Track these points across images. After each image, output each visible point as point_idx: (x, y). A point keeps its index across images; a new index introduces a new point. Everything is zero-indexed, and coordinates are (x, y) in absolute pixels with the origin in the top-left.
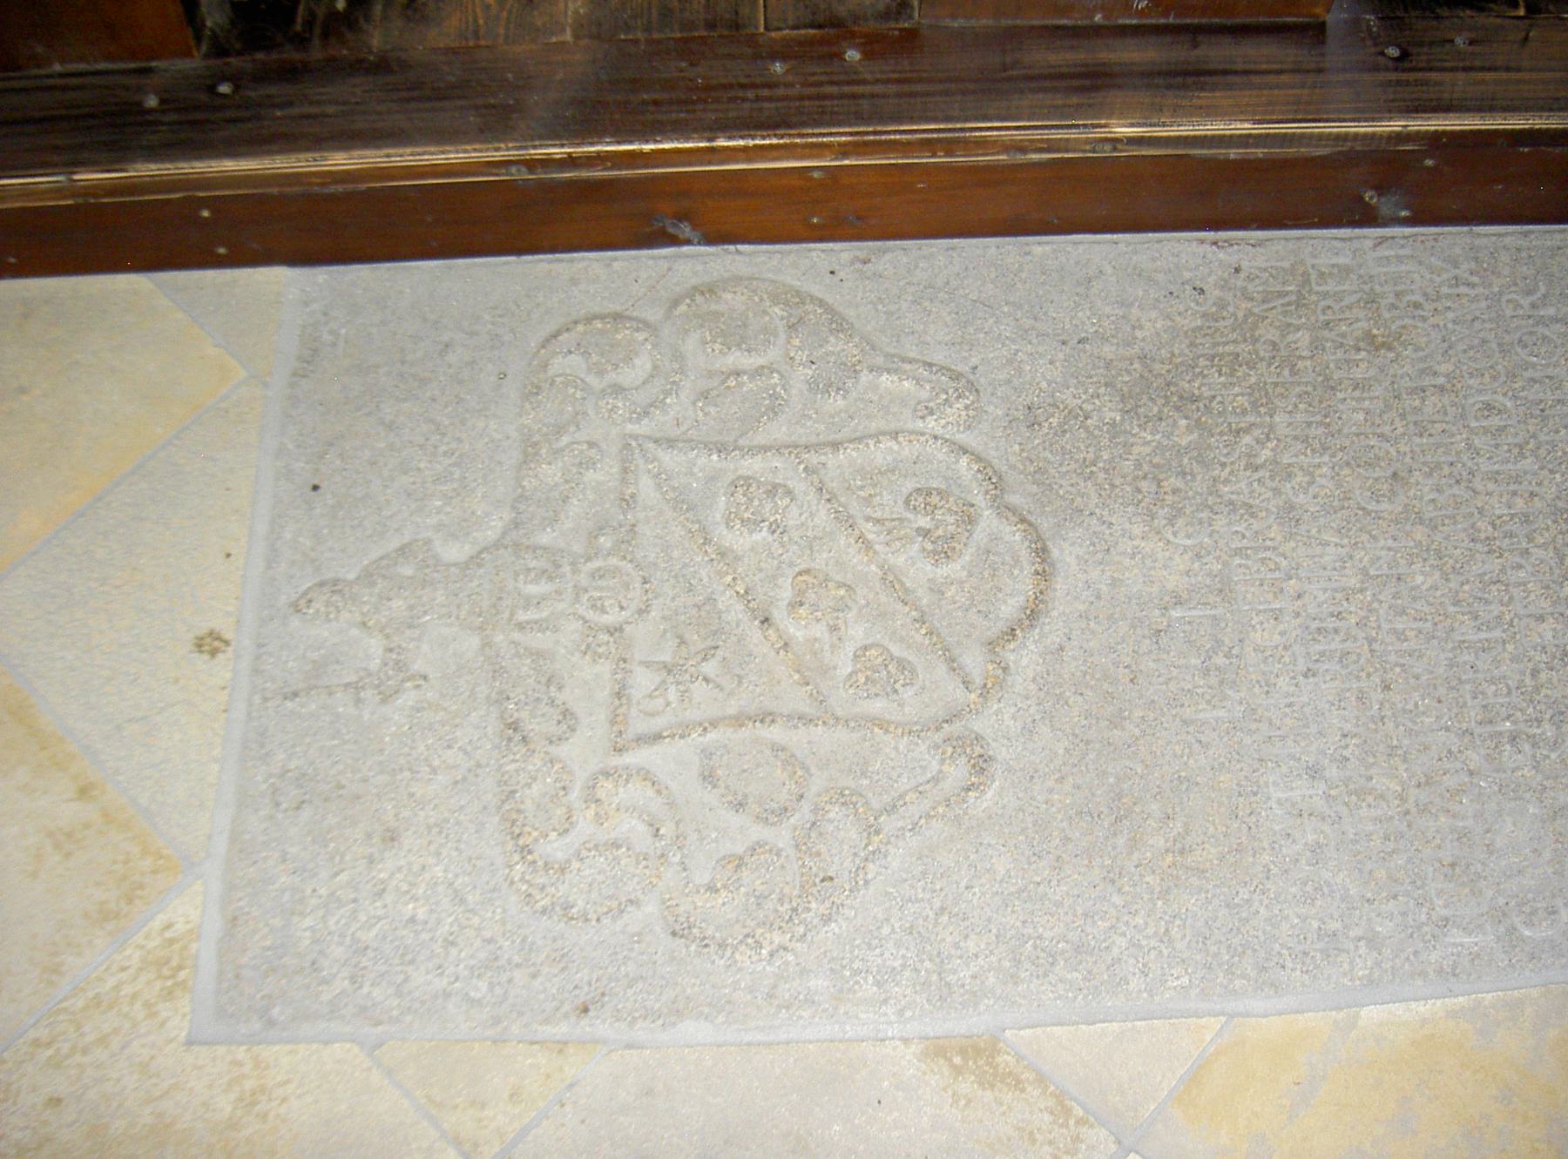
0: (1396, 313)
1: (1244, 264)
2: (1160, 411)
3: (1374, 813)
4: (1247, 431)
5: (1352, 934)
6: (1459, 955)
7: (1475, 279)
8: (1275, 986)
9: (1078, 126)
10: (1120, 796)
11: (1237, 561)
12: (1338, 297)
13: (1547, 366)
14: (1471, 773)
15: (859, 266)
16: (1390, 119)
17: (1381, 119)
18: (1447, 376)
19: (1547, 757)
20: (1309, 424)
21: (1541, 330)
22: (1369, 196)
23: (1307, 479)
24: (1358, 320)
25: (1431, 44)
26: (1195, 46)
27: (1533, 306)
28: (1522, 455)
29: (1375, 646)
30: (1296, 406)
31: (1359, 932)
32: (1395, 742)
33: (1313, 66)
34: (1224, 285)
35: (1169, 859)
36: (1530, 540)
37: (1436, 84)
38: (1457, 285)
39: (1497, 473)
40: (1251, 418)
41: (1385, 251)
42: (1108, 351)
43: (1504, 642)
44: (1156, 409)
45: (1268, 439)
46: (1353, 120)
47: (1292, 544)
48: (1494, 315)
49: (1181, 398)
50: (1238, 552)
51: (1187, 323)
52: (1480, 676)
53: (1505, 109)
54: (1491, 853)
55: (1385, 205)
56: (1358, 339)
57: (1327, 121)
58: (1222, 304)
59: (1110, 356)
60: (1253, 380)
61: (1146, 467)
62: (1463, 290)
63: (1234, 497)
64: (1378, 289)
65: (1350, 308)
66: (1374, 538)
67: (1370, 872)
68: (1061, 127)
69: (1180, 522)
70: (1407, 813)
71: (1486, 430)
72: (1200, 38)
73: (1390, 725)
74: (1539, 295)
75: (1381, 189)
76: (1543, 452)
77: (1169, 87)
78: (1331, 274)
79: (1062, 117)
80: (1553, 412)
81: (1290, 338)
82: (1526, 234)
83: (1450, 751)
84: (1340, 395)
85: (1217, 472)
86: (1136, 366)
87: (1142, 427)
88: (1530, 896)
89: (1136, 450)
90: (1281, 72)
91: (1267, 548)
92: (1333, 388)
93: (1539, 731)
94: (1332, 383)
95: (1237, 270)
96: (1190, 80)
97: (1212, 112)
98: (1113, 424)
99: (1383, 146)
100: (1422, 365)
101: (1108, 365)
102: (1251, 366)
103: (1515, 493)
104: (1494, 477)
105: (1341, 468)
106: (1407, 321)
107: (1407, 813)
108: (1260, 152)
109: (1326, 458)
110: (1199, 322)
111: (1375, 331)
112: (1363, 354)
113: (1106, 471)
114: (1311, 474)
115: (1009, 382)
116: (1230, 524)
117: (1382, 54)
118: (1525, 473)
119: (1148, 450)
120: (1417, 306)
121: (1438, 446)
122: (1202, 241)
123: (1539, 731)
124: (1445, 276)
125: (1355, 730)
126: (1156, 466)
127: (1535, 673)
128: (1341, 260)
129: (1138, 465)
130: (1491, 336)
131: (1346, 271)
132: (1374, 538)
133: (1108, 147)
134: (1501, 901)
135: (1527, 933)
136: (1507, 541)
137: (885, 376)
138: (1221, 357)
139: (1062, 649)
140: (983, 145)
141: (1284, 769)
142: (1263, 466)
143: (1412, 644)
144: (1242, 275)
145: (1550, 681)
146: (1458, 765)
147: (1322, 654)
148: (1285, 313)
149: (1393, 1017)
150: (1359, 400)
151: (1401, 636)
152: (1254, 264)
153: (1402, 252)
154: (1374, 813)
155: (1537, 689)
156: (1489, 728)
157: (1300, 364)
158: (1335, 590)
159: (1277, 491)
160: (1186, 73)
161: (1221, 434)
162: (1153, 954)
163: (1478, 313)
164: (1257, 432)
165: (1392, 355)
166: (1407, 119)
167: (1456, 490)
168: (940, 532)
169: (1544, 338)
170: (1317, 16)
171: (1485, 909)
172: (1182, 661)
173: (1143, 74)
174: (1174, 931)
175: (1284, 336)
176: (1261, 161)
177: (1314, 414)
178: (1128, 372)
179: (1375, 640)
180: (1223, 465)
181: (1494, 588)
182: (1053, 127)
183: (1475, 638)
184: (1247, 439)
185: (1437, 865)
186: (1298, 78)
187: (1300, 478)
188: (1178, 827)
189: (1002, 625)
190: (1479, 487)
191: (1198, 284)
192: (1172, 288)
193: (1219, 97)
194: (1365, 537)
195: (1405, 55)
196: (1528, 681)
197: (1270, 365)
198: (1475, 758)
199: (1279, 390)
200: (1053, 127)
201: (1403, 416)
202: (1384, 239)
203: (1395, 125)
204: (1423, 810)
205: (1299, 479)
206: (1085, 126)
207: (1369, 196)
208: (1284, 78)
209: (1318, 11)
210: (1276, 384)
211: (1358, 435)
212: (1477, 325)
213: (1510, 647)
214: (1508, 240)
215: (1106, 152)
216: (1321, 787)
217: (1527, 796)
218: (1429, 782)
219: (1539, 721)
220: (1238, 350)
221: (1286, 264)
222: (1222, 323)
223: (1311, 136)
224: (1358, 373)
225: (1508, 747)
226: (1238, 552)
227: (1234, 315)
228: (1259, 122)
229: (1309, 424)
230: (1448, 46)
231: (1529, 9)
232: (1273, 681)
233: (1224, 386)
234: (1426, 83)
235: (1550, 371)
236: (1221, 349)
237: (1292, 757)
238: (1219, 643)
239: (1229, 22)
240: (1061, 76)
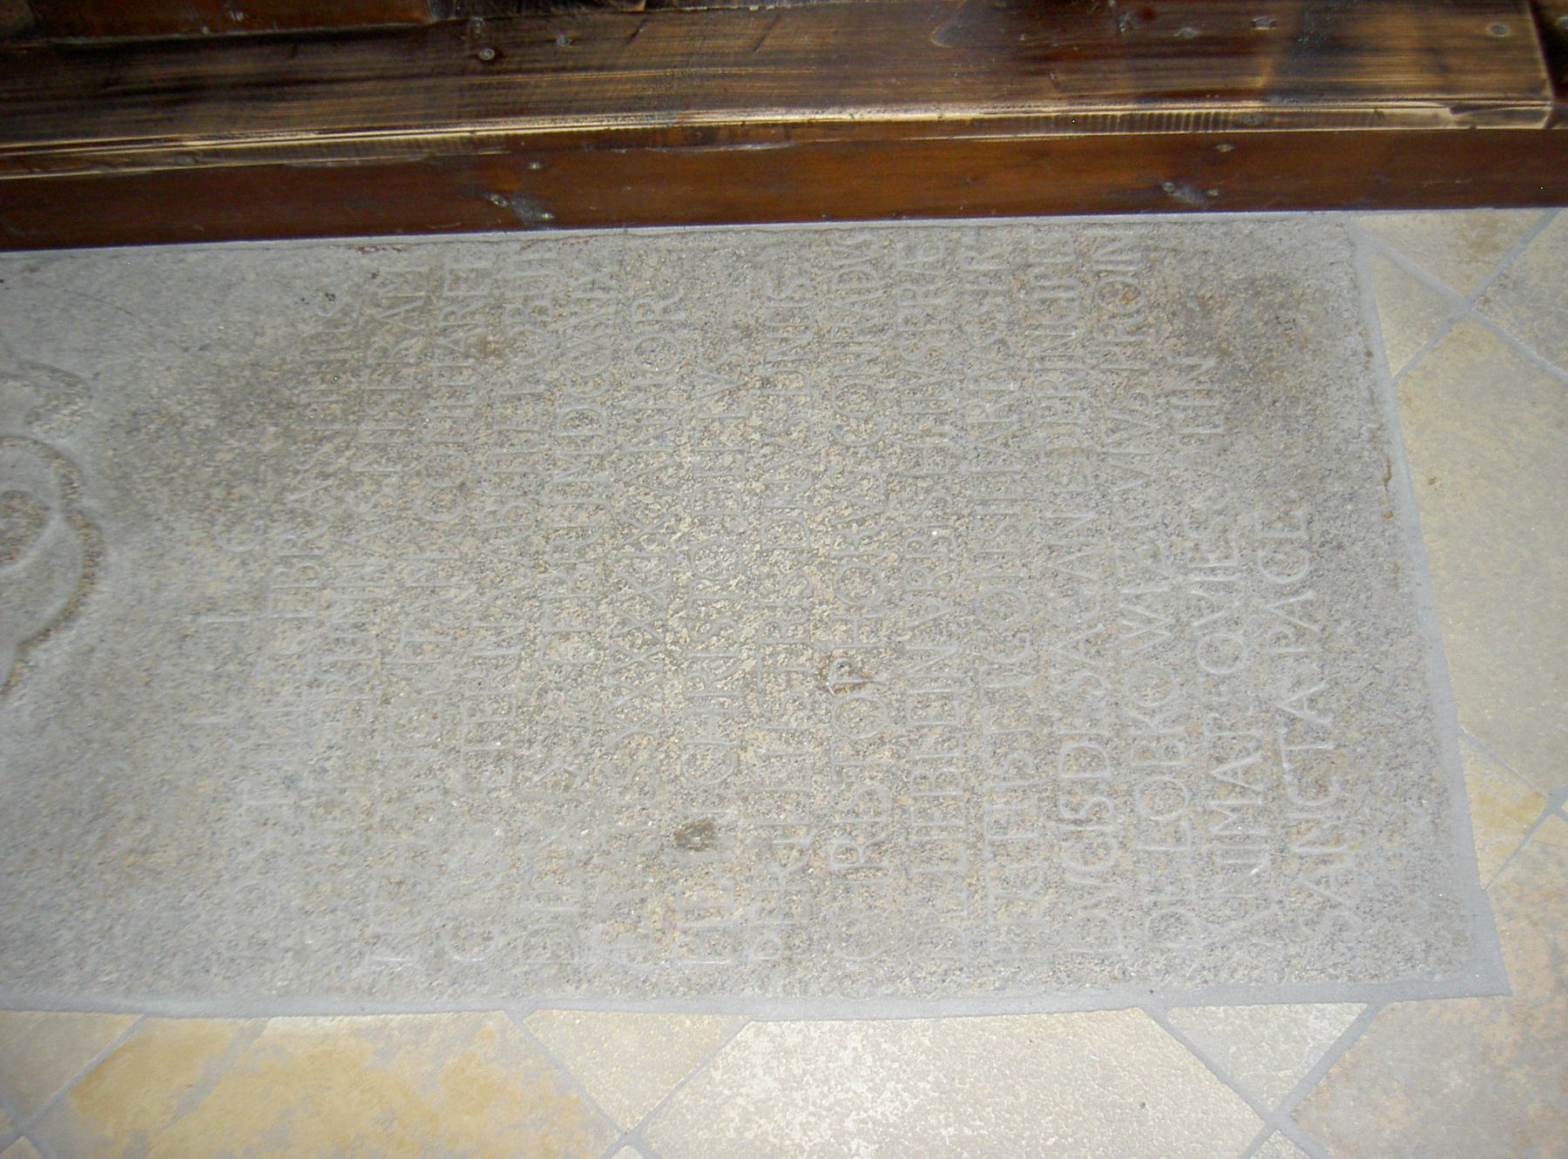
0: (518, 319)
1: (383, 270)
2: (253, 419)
3: (337, 825)
4: (329, 439)
5: (282, 945)
6: (380, 973)
7: (613, 283)
8: (195, 988)
9: (150, 141)
10: (103, 796)
11: (280, 569)
12: (463, 302)
13: (660, 373)
14: (446, 792)
15: (27, 274)
16: (456, 125)
17: (447, 125)
18: (548, 384)
19: (529, 779)
20: (392, 432)
21: (667, 336)
22: (1168, 186)
23: (374, 488)
24: (476, 326)
25: (532, 43)
26: (293, 54)
27: (665, 311)
28: (601, 467)
29: (388, 659)
30: (386, 414)
31: (289, 942)
32: (378, 757)
33: (400, 72)
34: (356, 292)
35: (131, 859)
36: (581, 553)
37: (520, 86)
38: (592, 290)
39: (569, 485)
40: (338, 426)
41: (530, 255)
42: (225, 358)
43: (520, 660)
44: (250, 416)
45: (348, 448)
46: (418, 127)
47: (339, 553)
48: (619, 321)
49: (278, 404)
50: (284, 560)
51: (308, 330)
52: (485, 693)
53: (580, 111)
54: (443, 874)
55: (1185, 194)
56: (470, 346)
57: (405, 127)
58: (346, 312)
59: (226, 363)
60: (353, 387)
61: (223, 474)
62: (599, 294)
63: (297, 505)
64: (509, 294)
65: (473, 314)
66: (421, 549)
67: (317, 885)
68: (137, 142)
69: (237, 529)
70: (369, 828)
71: (571, 440)
72: (302, 47)
73: (378, 738)
74: (676, 298)
75: (1177, 180)
76: (623, 464)
77: (251, 99)
78: (467, 279)
79: (141, 132)
80: (651, 421)
81: (405, 344)
82: (683, 235)
83: (430, 769)
84: (433, 403)
85: (287, 480)
86: (247, 373)
87: (232, 434)
88: (469, 920)
89: (219, 457)
90: (367, 79)
91: (314, 557)
92: (429, 396)
93: (527, 753)
94: (430, 391)
95: (374, 276)
96: (274, 91)
97: (281, 123)
98: (207, 431)
99: (463, 152)
100: (526, 373)
101: (221, 371)
102: (355, 373)
103: (580, 506)
104: (564, 489)
105: (411, 478)
106: (528, 327)
107: (369, 828)
108: (356, 160)
109: (399, 467)
110: (320, 329)
111: (491, 338)
112: (471, 361)
113: (185, 477)
114: (379, 484)
115: (123, 388)
116: (285, 531)
117: (476, 57)
118: (599, 485)
119: (229, 457)
120: (542, 311)
121: (516, 456)
122: (349, 247)
123: (527, 753)
124: (583, 280)
125: (343, 743)
126: (234, 473)
127: (543, 692)
128: (483, 264)
129: (216, 473)
130: (606, 342)
131: (482, 275)
132: (421, 549)
133: (188, 160)
134: (437, 923)
135: (456, 957)
136: (556, 556)
137: (11, 383)
138: (329, 363)
139: (92, 650)
140: (68, 161)
141: (264, 777)
142: (334, 474)
143: (427, 658)
144: (377, 281)
145: (555, 701)
146: (434, 783)
147: (333, 665)
148: (405, 320)
149: (295, 1029)
150: (450, 408)
151: (417, 649)
152: (394, 269)
153: (547, 255)
154: (337, 825)
155: (540, 710)
156: (479, 747)
157: (405, 371)
158: (365, 601)
159: (339, 500)
160: (270, 85)
161: (305, 441)
162: (94, 948)
163: (603, 319)
164: (338, 441)
165: (499, 362)
166: (472, 124)
167: (521, 503)
168: (10, 535)
169: (666, 344)
170: (418, 21)
171: (418, 929)
172: (199, 667)
173: (234, 87)
174: (117, 930)
175: (397, 343)
176: (359, 168)
177: (400, 422)
178: (237, 378)
179: (390, 653)
180: (297, 472)
181: (527, 604)
182: (131, 142)
183: (494, 653)
184: (327, 447)
185: (384, 882)
186: (381, 85)
187: (367, 487)
188: (148, 828)
189: (40, 626)
190: (546, 500)
191: (332, 290)
192: (306, 294)
193: (297, 108)
194: (412, 548)
195: (499, 56)
196: (533, 701)
197: (374, 371)
198: (454, 777)
199: (375, 398)
200: (131, 142)
201: (489, 426)
202: (534, 242)
203: (463, 131)
204: (386, 825)
205: (365, 488)
206: (159, 140)
207: (1168, 186)
208: (367, 86)
209: (416, 15)
210: (373, 392)
211: (437, 444)
212: (599, 332)
213: (525, 665)
214: (661, 242)
215: (187, 165)
216: (292, 797)
217: (496, 818)
218: (402, 795)
219: (531, 743)
220: (348, 356)
221: (424, 270)
222: (343, 330)
223: (381, 144)
224: (459, 381)
225: (491, 767)
226: (284, 560)
227: (357, 321)
228: (325, 131)
229: (392, 432)
230: (548, 47)
231: (649, 5)
232: (278, 689)
233: (323, 393)
234: (509, 86)
235: (659, 379)
236: (331, 356)
237: (272, 766)
238: (237, 649)
239: (334, 30)
240: (156, 91)
